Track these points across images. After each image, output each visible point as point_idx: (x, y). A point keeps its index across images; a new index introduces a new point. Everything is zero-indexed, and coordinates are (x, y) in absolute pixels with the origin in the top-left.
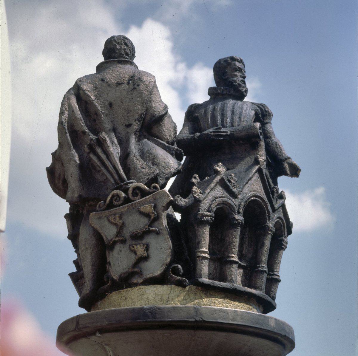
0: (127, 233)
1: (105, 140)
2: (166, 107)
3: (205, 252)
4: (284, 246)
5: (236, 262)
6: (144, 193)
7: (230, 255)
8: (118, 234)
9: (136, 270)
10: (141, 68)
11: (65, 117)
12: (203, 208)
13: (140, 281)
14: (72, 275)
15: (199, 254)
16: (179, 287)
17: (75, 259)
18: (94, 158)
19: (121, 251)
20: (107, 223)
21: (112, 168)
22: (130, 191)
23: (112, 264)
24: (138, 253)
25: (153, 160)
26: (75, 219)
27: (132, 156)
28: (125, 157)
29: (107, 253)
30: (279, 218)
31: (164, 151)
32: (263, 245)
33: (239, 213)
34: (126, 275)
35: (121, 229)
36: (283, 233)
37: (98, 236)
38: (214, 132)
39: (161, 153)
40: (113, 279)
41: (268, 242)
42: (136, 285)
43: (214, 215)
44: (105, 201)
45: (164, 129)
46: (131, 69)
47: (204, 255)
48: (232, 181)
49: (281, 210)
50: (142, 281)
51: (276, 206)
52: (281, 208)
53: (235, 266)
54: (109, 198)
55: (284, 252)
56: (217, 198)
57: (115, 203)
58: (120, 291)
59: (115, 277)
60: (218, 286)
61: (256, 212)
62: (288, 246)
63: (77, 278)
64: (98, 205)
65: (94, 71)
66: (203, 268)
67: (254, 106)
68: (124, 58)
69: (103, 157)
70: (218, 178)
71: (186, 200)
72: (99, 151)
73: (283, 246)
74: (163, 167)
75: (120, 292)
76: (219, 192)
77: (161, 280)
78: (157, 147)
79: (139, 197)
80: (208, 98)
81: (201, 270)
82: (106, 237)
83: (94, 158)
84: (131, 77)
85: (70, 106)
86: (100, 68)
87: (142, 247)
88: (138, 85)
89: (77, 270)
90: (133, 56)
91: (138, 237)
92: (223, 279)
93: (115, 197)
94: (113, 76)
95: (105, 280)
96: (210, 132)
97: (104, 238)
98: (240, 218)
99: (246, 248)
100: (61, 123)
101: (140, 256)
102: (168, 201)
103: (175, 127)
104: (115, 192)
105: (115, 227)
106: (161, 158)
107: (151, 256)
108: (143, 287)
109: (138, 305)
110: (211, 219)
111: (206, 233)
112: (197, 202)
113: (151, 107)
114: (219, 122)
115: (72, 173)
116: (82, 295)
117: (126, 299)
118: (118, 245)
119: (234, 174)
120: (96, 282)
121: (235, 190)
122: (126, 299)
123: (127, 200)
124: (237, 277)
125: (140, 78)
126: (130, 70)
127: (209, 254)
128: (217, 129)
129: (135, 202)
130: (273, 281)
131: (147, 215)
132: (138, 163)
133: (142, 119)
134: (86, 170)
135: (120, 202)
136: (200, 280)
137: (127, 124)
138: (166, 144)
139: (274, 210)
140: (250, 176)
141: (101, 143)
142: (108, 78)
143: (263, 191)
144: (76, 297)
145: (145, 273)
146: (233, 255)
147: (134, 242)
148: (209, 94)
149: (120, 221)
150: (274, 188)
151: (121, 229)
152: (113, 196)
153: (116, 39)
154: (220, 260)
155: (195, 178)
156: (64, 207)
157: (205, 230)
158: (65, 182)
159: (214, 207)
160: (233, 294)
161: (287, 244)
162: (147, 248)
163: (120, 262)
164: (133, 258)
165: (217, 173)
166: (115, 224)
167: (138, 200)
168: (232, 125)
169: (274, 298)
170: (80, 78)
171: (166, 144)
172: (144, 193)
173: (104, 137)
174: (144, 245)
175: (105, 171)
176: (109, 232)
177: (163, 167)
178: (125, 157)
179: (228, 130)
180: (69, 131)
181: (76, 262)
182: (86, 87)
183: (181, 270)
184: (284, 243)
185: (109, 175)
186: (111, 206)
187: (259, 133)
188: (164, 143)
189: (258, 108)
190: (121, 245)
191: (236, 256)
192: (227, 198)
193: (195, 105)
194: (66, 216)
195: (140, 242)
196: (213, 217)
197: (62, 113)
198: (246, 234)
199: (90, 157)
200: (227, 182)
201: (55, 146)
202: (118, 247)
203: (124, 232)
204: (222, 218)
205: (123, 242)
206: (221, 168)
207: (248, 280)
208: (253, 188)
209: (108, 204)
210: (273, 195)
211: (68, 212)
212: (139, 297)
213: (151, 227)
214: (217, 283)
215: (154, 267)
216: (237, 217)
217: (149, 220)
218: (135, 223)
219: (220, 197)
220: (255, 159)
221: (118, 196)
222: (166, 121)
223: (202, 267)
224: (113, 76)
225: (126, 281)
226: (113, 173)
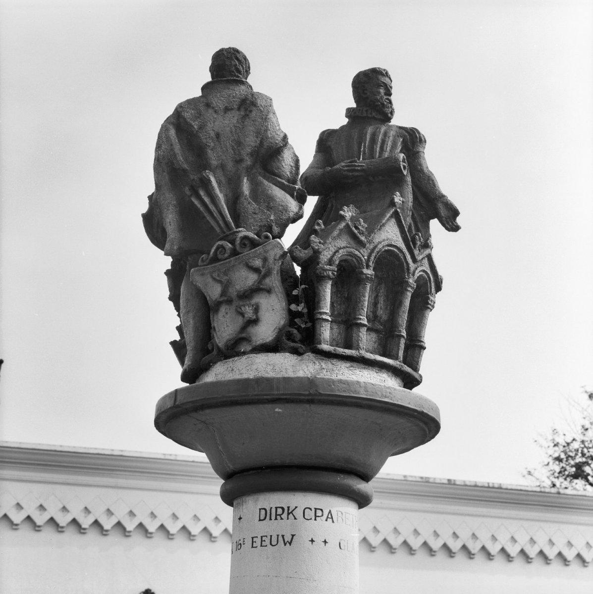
0: (233, 292)
1: (209, 181)
2: (285, 137)
3: (326, 313)
4: (430, 305)
5: (364, 325)
6: (254, 244)
7: (357, 317)
8: (224, 293)
9: (244, 335)
10: (256, 89)
12: (325, 256)
13: (249, 348)
14: (174, 344)
15: (319, 316)
16: (295, 355)
17: (178, 325)
18: (196, 202)
19: (227, 313)
20: (210, 280)
21: (218, 214)
22: (238, 241)
23: (217, 329)
24: (246, 316)
25: (269, 202)
26: (175, 276)
27: (242, 199)
28: (234, 201)
29: (211, 316)
30: (424, 271)
31: (283, 192)
32: (401, 303)
33: (368, 267)
34: (232, 342)
35: (226, 287)
36: (429, 290)
37: (202, 297)
38: (346, 166)
39: (278, 193)
40: (219, 349)
42: (244, 353)
43: (336, 269)
44: (209, 254)
45: (283, 164)
46: (243, 91)
47: (324, 317)
48: (360, 227)
49: (426, 261)
50: (250, 348)
51: (419, 258)
52: (426, 259)
53: (364, 330)
54: (213, 251)
55: (431, 313)
56: (340, 248)
57: (220, 256)
58: (226, 361)
59: (220, 345)
60: (340, 354)
61: (391, 266)
62: (436, 305)
63: (179, 348)
64: (200, 259)
65: (198, 93)
66: (323, 333)
67: (401, 130)
68: (235, 76)
69: (207, 200)
70: (342, 225)
71: (306, 251)
73: (429, 306)
74: (280, 211)
75: (226, 362)
76: (342, 242)
77: (272, 348)
78: (274, 187)
79: (248, 249)
80: (345, 121)
81: (320, 335)
82: (210, 297)
83: (196, 202)
84: (243, 101)
85: (168, 138)
87: (251, 308)
88: (251, 111)
89: (181, 338)
90: (248, 72)
91: (247, 295)
92: (348, 346)
93: (220, 249)
94: (221, 100)
95: (210, 348)
96: (342, 167)
97: (208, 298)
98: (369, 272)
99: (381, 309)
101: (248, 319)
102: (281, 253)
104: (220, 243)
105: (219, 285)
106: (278, 200)
107: (261, 319)
108: (252, 355)
109: (245, 376)
110: (333, 273)
111: (327, 292)
112: (317, 253)
113: (267, 138)
114: (355, 153)
115: (171, 220)
116: (185, 366)
117: (233, 370)
118: (223, 307)
119: (332, 222)
120: (199, 349)
121: (363, 238)
122: (233, 370)
123: (234, 253)
125: (253, 102)
126: (241, 91)
127: (330, 316)
128: (350, 162)
129: (242, 255)
130: (415, 346)
131: (256, 270)
132: (249, 206)
133: (255, 154)
135: (226, 255)
136: (319, 346)
137: (238, 159)
138: (286, 183)
140: (384, 221)
141: (206, 184)
142: (214, 102)
143: (400, 239)
144: (178, 370)
145: (254, 339)
146: (361, 317)
147: (241, 303)
148: (346, 116)
149: (225, 278)
150: (416, 234)
151: (226, 287)
152: (218, 248)
153: (225, 53)
154: (347, 323)
155: (319, 224)
156: (167, 262)
157: (325, 287)
158: (164, 232)
161: (434, 303)
162: (257, 309)
163: (225, 327)
164: (240, 321)
165: (343, 218)
166: (220, 282)
167: (247, 253)
168: (372, 155)
169: (416, 369)
170: (181, 103)
171: (286, 183)
172: (254, 244)
173: (208, 176)
174: (253, 306)
175: (209, 218)
176: (214, 292)
177: (280, 211)
178: (234, 201)
179: (361, 162)
180: (166, 167)
181: (179, 329)
182: (188, 115)
183: (299, 336)
184: (430, 302)
185: (213, 220)
186: (215, 259)
187: (402, 167)
188: (284, 181)
189: (406, 134)
190: (227, 307)
191: (365, 318)
192: (353, 248)
193: (327, 132)
194: (168, 273)
195: (248, 302)
196: (335, 271)
198: (381, 291)
199: (192, 201)
200: (354, 229)
202: (223, 309)
203: (230, 290)
204: (348, 275)
205: (229, 302)
206: (348, 213)
208: (390, 234)
209: (212, 258)
210: (415, 244)
211: (170, 268)
212: (248, 368)
213: (262, 284)
214: (341, 351)
215: (265, 331)
216: (365, 271)
217: (259, 277)
218: (245, 279)
219: (344, 248)
221: (222, 247)
223: (322, 331)
224: (221, 100)
225: (232, 351)
226: (219, 220)
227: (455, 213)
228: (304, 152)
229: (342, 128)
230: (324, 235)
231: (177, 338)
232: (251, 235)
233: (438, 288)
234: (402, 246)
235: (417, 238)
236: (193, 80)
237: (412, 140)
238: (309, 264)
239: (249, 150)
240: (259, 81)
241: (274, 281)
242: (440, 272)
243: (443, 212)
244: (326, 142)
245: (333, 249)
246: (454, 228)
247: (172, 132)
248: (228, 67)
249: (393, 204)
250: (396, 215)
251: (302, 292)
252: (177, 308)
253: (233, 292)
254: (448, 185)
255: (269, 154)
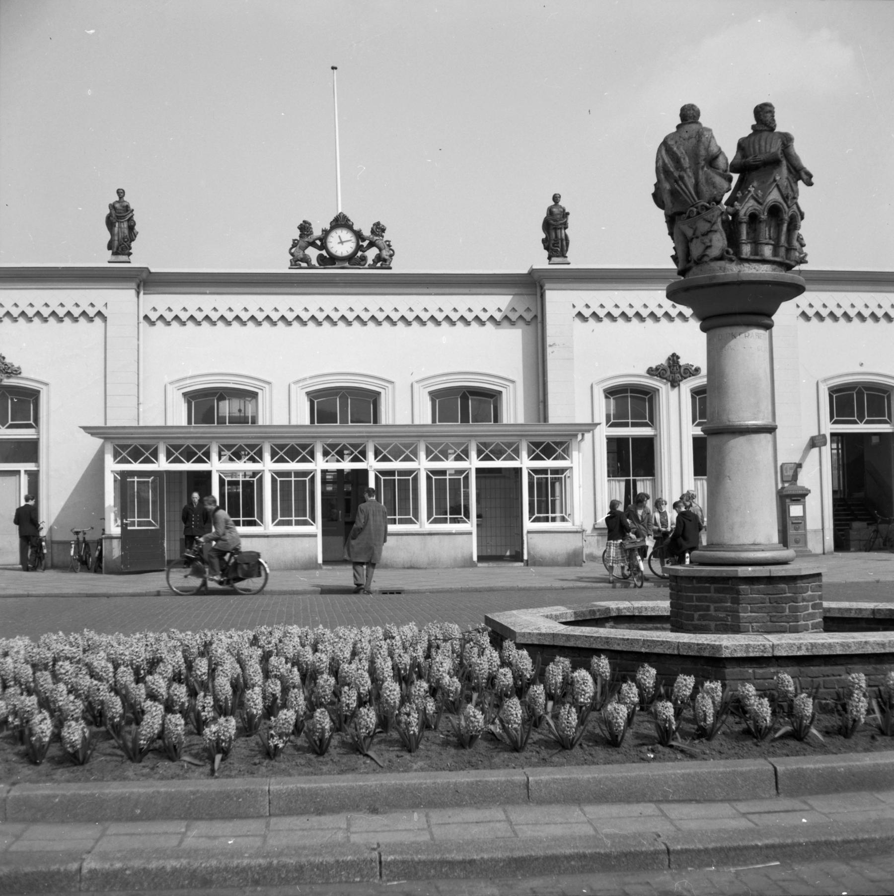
2: (720, 149)
8: (694, 234)
10: (704, 125)
11: (660, 162)
12: (742, 213)
14: (672, 257)
25: (714, 185)
28: (697, 185)
37: (685, 235)
41: (785, 228)
65: (675, 130)
69: (683, 187)
72: (680, 183)
86: (678, 127)
92: (757, 254)
100: (657, 169)
103: (727, 160)
111: (744, 229)
115: (667, 198)
124: (767, 251)
132: (704, 188)
134: (674, 193)
139: (789, 207)
159: (748, 214)
160: (764, 261)
163: (696, 250)
167: (704, 213)
176: (690, 233)
180: (662, 171)
182: (670, 143)
186: (689, 217)
197: (657, 162)
201: (655, 181)
202: (695, 241)
204: (753, 218)
205: (697, 238)
207: (775, 253)
208: (774, 196)
218: (703, 226)
220: (264, 706)
222: (721, 158)
225: (699, 261)
227: (811, 176)
228: (730, 153)
229: (750, 135)
230: (741, 200)
231: (673, 253)
232: (706, 204)
233: (802, 218)
234: (782, 201)
235: (790, 197)
236: (671, 123)
237: (787, 140)
238: (735, 214)
239: (702, 158)
240: (704, 120)
241: (719, 226)
242: (803, 209)
243: (805, 177)
244: (742, 146)
245: (746, 207)
246: (809, 184)
247: (663, 152)
248: (689, 115)
249: (775, 180)
250: (777, 186)
251: (731, 229)
252: (673, 239)
253: (698, 233)
254: (807, 161)
255: (712, 160)
